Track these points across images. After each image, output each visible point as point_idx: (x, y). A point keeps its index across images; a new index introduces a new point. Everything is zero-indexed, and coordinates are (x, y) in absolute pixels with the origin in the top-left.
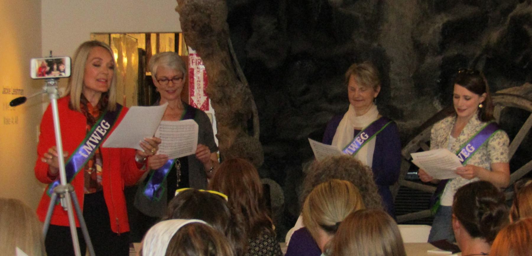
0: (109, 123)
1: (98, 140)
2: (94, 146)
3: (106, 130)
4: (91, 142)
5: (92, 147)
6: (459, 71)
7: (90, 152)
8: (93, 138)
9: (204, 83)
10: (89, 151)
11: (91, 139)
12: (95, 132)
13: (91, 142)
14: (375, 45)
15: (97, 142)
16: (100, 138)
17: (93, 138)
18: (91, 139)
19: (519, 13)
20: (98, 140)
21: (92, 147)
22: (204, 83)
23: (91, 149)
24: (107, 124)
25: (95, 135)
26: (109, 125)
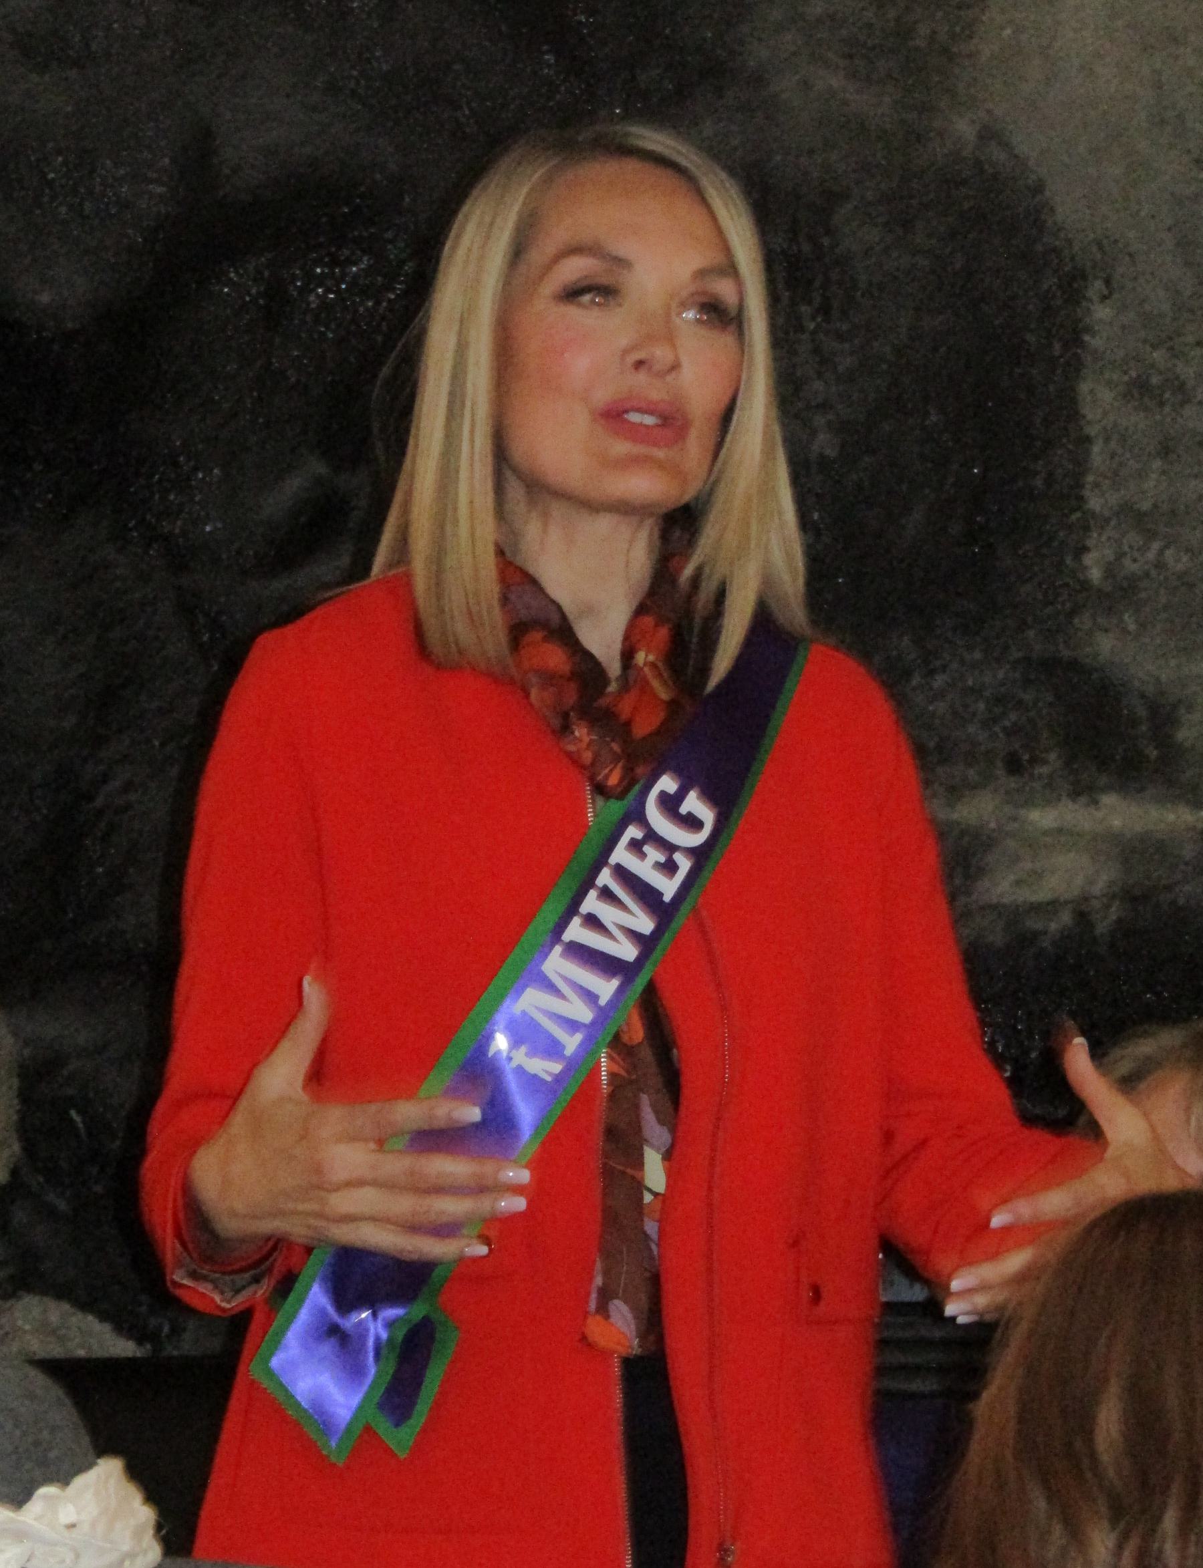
0: (710, 796)
2: (606, 988)
3: (692, 852)
5: (590, 997)
7: (578, 1037)
8: (592, 921)
10: (572, 1025)
11: (576, 931)
12: (605, 878)
15: (628, 951)
16: (645, 924)
18: (576, 931)
21: (590, 997)
23: (585, 1015)
24: (693, 804)
25: (607, 895)
26: (707, 815)
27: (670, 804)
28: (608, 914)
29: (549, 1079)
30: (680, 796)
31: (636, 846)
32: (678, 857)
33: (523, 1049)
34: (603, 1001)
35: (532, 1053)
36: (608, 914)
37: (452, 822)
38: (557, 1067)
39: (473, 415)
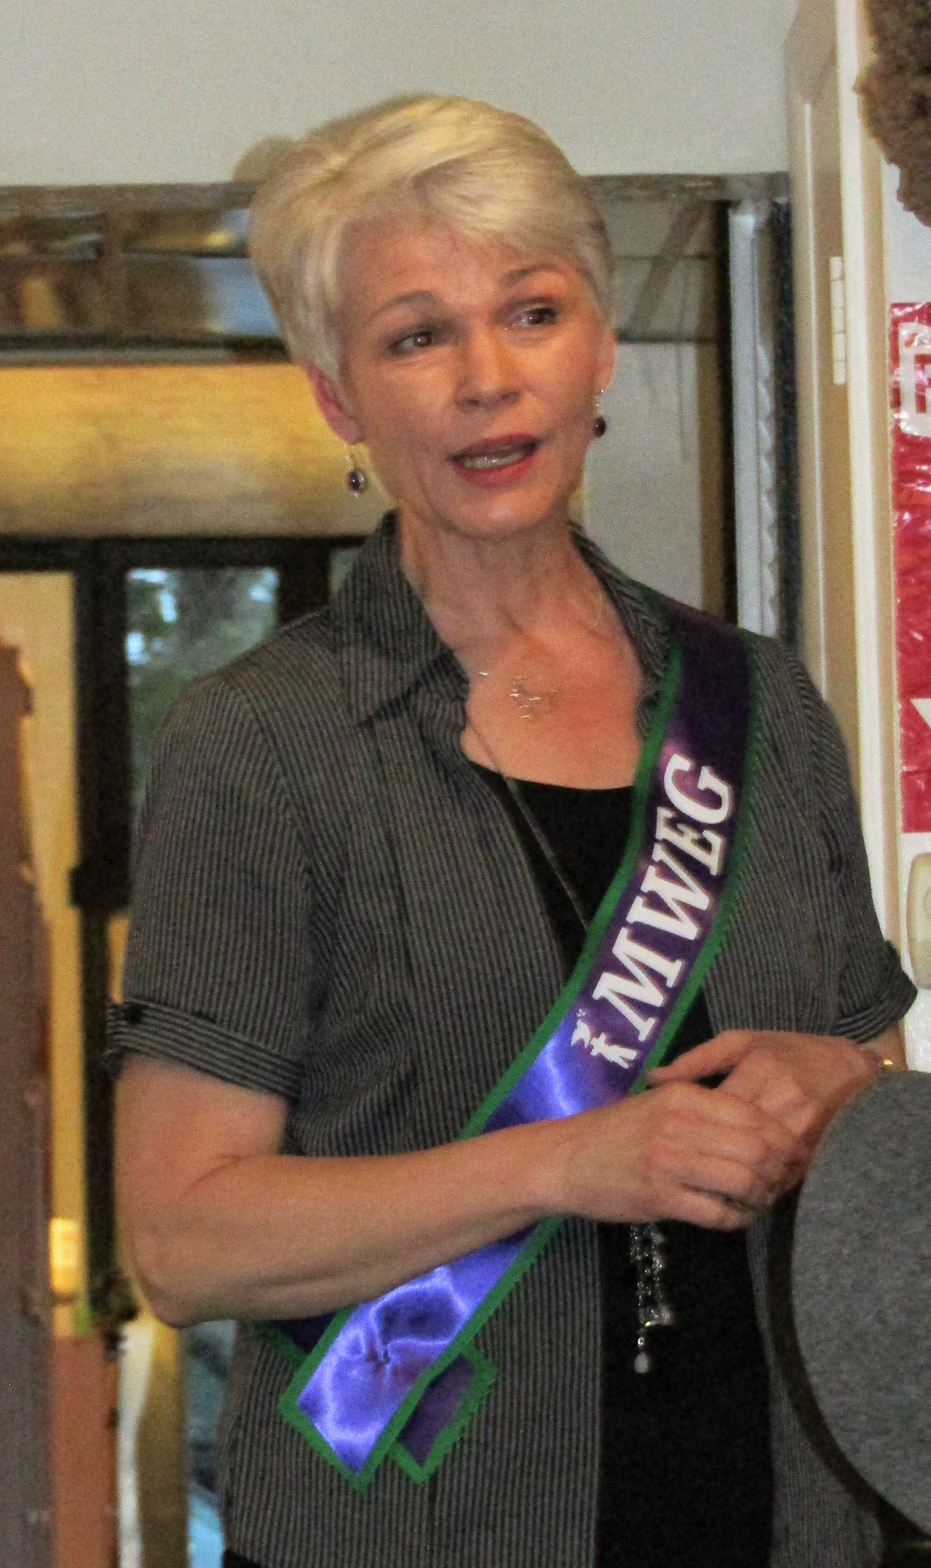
0: (722, 773)
1: (693, 912)
2: (672, 970)
3: (717, 828)
4: (643, 934)
5: (658, 979)
6: (885, 1069)
7: (652, 1022)
8: (655, 902)
9: (235, 593)
10: (644, 1009)
11: (639, 912)
12: (659, 854)
13: (643, 934)
14: (902, 450)
15: (688, 930)
16: (701, 899)
17: (655, 902)
18: (639, 912)
19: (588, 239)
20: (693, 912)
21: (658, 979)
22: (235, 593)
23: (655, 998)
24: (708, 780)
25: (666, 873)
26: (722, 789)
27: (687, 782)
28: (668, 891)
29: (625, 1066)
30: (695, 773)
31: (673, 823)
32: (709, 835)
33: (603, 1037)
34: (670, 983)
35: (613, 1041)
36: (668, 891)
37: (28, 941)
38: (632, 1054)
39: (680, 377)
